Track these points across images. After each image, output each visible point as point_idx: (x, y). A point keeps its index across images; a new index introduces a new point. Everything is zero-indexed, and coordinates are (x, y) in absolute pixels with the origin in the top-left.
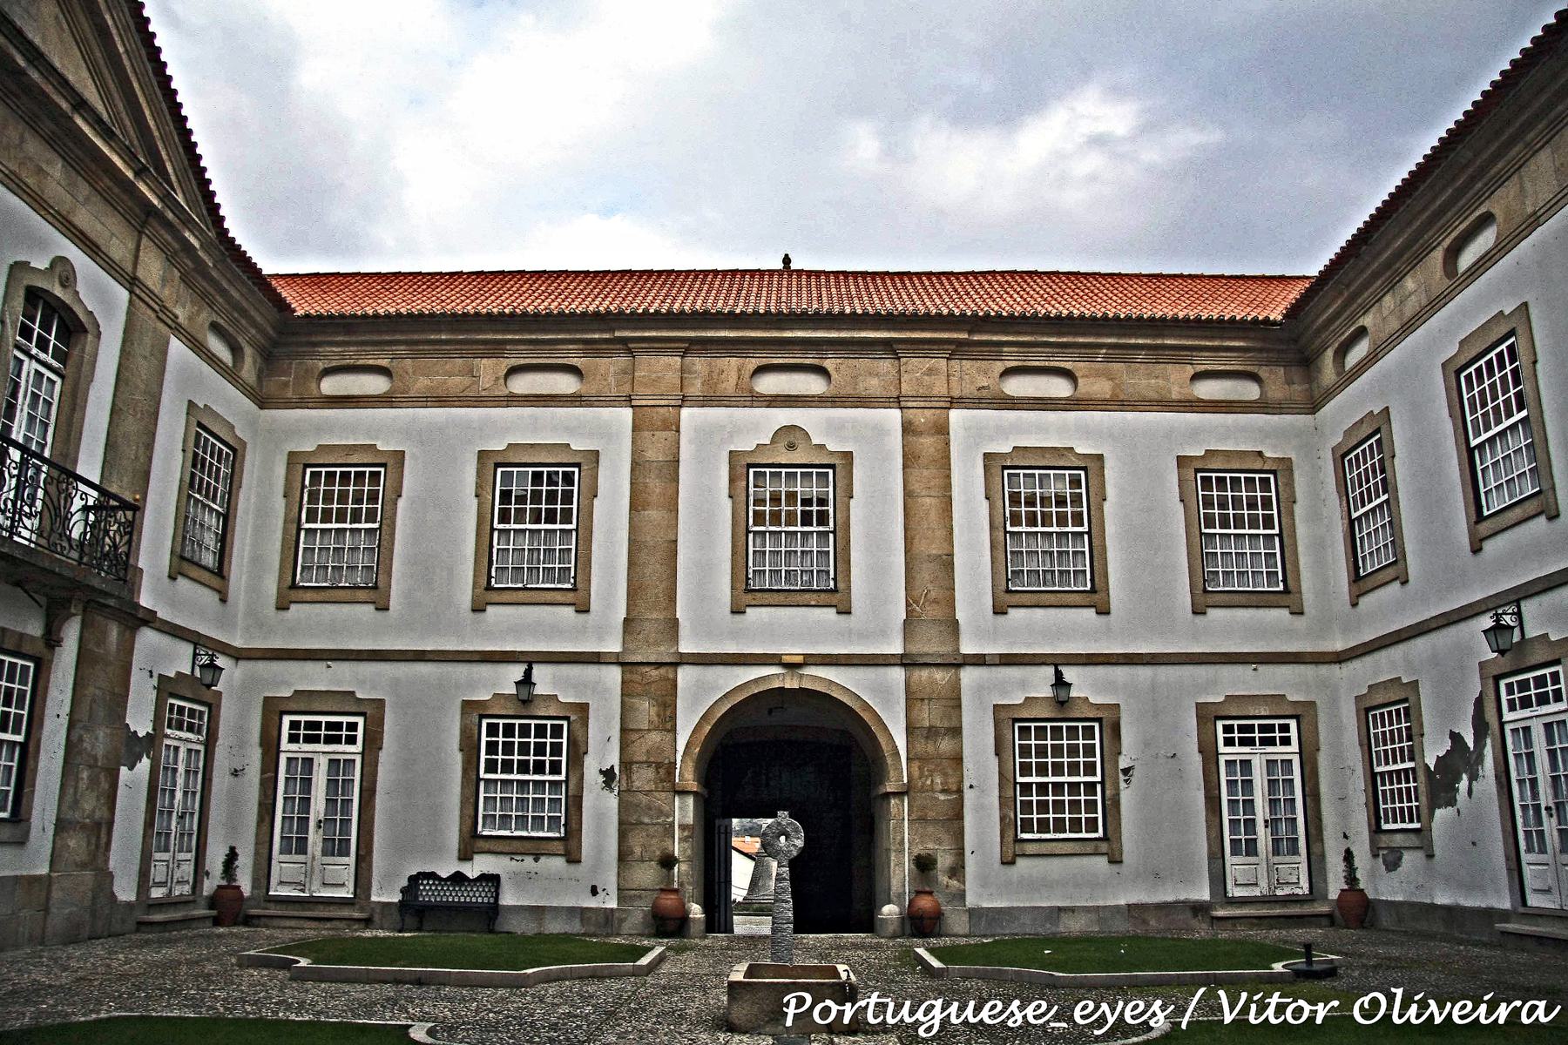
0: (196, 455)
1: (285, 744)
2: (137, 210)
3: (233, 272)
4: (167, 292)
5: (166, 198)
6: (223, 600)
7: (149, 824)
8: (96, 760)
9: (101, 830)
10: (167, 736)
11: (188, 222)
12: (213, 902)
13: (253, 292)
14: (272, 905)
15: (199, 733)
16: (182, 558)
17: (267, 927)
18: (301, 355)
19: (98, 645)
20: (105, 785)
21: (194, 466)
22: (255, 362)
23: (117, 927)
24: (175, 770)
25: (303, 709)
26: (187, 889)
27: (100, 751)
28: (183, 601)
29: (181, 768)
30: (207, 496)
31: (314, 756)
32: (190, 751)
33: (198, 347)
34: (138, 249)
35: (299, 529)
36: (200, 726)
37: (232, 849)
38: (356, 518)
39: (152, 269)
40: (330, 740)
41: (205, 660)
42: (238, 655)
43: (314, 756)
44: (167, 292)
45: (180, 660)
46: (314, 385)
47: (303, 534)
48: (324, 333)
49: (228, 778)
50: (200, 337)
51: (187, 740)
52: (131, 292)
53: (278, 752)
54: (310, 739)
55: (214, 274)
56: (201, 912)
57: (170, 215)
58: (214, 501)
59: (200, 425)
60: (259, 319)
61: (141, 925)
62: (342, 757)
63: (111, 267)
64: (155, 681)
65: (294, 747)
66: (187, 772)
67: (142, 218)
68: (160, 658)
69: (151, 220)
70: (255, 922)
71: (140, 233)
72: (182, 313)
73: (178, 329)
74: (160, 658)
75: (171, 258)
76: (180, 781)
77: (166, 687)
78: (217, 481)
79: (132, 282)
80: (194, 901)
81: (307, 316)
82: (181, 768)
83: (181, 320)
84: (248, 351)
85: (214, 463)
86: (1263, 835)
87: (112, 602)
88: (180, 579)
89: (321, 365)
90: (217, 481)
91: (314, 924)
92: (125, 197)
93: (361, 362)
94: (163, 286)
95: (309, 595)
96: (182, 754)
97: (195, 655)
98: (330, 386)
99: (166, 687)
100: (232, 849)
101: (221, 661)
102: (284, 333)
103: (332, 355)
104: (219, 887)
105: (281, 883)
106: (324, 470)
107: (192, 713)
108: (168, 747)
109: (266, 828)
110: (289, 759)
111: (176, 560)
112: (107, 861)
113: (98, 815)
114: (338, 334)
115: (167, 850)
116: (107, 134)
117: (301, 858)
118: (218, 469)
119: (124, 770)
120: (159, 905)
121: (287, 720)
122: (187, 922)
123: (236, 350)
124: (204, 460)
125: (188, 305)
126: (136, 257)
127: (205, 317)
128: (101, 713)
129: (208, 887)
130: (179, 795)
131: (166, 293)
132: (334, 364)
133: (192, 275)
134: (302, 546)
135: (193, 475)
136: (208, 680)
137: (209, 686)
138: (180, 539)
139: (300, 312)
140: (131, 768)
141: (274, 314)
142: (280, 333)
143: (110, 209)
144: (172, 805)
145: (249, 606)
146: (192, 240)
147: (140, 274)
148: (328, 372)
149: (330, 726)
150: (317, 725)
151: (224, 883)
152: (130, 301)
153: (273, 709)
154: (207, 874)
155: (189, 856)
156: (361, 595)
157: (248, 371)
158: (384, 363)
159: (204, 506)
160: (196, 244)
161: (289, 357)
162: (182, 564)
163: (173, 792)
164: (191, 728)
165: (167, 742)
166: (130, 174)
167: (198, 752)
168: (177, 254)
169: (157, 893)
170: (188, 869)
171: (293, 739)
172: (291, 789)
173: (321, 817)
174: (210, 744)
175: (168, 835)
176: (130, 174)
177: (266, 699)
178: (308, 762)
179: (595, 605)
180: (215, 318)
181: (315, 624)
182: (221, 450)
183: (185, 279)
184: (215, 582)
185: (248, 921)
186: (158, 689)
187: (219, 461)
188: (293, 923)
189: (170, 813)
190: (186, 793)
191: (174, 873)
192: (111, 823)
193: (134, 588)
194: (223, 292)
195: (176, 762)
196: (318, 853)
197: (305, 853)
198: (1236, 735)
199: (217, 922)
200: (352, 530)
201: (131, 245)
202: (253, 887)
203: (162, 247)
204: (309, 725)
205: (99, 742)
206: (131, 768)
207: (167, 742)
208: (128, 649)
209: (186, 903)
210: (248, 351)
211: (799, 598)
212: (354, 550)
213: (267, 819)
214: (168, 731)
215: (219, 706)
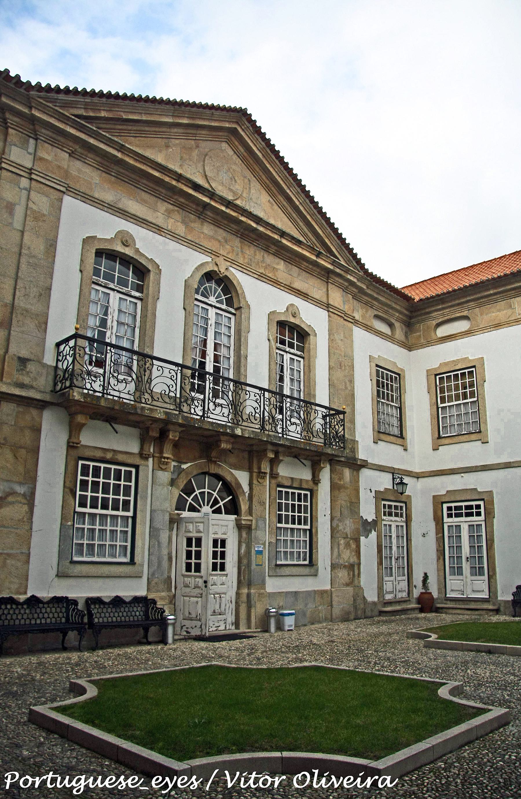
0: (378, 381)
1: (446, 519)
2: (323, 273)
3: (378, 288)
4: (346, 307)
5: (333, 263)
6: (405, 450)
7: (380, 563)
8: (347, 534)
9: (354, 568)
10: (383, 520)
11: (347, 271)
12: (419, 600)
13: (391, 296)
14: (448, 602)
15: (402, 516)
16: (379, 432)
17: (446, 613)
18: (424, 320)
19: (340, 479)
20: (354, 546)
21: (378, 386)
22: (402, 329)
23: (369, 614)
24: (391, 536)
25: (463, 499)
26: (404, 595)
27: (348, 530)
28: (386, 454)
29: (394, 535)
30: (388, 400)
31: (461, 524)
32: (397, 526)
33: (368, 328)
34: (328, 290)
35: (438, 408)
36: (402, 514)
37: (426, 574)
38: (465, 397)
39: (337, 297)
40: (468, 515)
41: (398, 480)
42: (418, 476)
43: (461, 524)
44: (346, 307)
45: (385, 482)
46: (433, 334)
47: (440, 409)
48: (433, 306)
49: (421, 538)
50: (369, 324)
51: (395, 521)
52: (328, 311)
53: (443, 523)
54: (457, 515)
55: (369, 292)
56: (414, 605)
57: (338, 270)
58: (392, 401)
59: (377, 366)
60: (398, 307)
61: (381, 613)
62: (454, 524)
63: (317, 303)
64: (373, 494)
65: (450, 520)
66: (398, 537)
67: (326, 275)
68: (373, 482)
69: (331, 275)
70: (441, 611)
71: (327, 282)
72: (357, 316)
73: (356, 322)
74: (373, 482)
75: (345, 290)
76: (394, 541)
77: (379, 496)
78: (392, 391)
79: (327, 307)
80: (409, 600)
81: (421, 300)
82: (394, 535)
83: (357, 318)
84: (397, 325)
85: (388, 384)
86: (466, 567)
87: (343, 459)
88: (379, 442)
89: (434, 323)
90: (392, 391)
91: (469, 612)
92: (315, 268)
93: (453, 316)
94: (344, 304)
95: (447, 441)
96: (393, 529)
97: (393, 479)
98: (442, 332)
99: (379, 496)
100: (426, 574)
101: (406, 480)
102: (414, 312)
103: (438, 316)
104: (422, 593)
105: (452, 590)
106: (445, 375)
107: (396, 507)
108: (385, 525)
109: (441, 561)
110: (448, 526)
111: (376, 433)
112: (359, 582)
113: (352, 561)
114: (438, 304)
115: (391, 575)
116: (298, 242)
117: (460, 577)
118: (392, 386)
119: (362, 539)
120: (389, 603)
121: (445, 506)
122: (404, 611)
123: (391, 325)
124: (383, 382)
125: (360, 310)
126: (328, 295)
127: (371, 312)
128: (346, 512)
129: (416, 593)
130: (394, 548)
131: (346, 308)
132: (440, 320)
133: (358, 295)
134: (440, 416)
135: (378, 391)
136: (400, 491)
137: (402, 494)
138: (376, 423)
139: (417, 299)
140: (367, 537)
141: (405, 303)
142: (411, 312)
143: (308, 275)
144: (391, 553)
145: (419, 450)
146: (352, 278)
147: (331, 302)
148: (438, 325)
149: (467, 507)
150: (460, 508)
151: (424, 591)
152: (329, 316)
153: (438, 502)
154: (415, 587)
155: (404, 578)
156: (473, 437)
157: (399, 334)
158: (465, 313)
159: (387, 405)
160: (355, 280)
161: (418, 322)
162: (381, 434)
163: (391, 547)
164: (396, 515)
165: (384, 523)
166: (314, 258)
167: (402, 526)
168: (348, 287)
169: (388, 597)
170: (404, 585)
171: (450, 516)
172: (451, 541)
173: (468, 555)
174: (408, 521)
175: (391, 568)
176: (314, 258)
177: (434, 497)
178: (458, 527)
179: (409, 448)
180: (376, 313)
181: (452, 455)
182: (391, 376)
183: (354, 297)
184: (400, 441)
185: (437, 610)
186: (376, 497)
187: (392, 381)
188: (459, 611)
189: (391, 558)
190: (398, 547)
191: (396, 586)
192: (359, 564)
193: (354, 450)
194: (376, 299)
195: (390, 532)
196: (469, 575)
197: (462, 574)
198: (453, 512)
199: (422, 610)
200: (464, 404)
201: (325, 290)
202: (439, 593)
203: (340, 286)
204: (456, 508)
205: (348, 526)
206: (367, 537)
207: (384, 523)
208: (356, 481)
209: (405, 601)
210: (397, 325)
211: (456, 439)
212: (467, 414)
213: (442, 558)
214: (384, 518)
215: (411, 503)
